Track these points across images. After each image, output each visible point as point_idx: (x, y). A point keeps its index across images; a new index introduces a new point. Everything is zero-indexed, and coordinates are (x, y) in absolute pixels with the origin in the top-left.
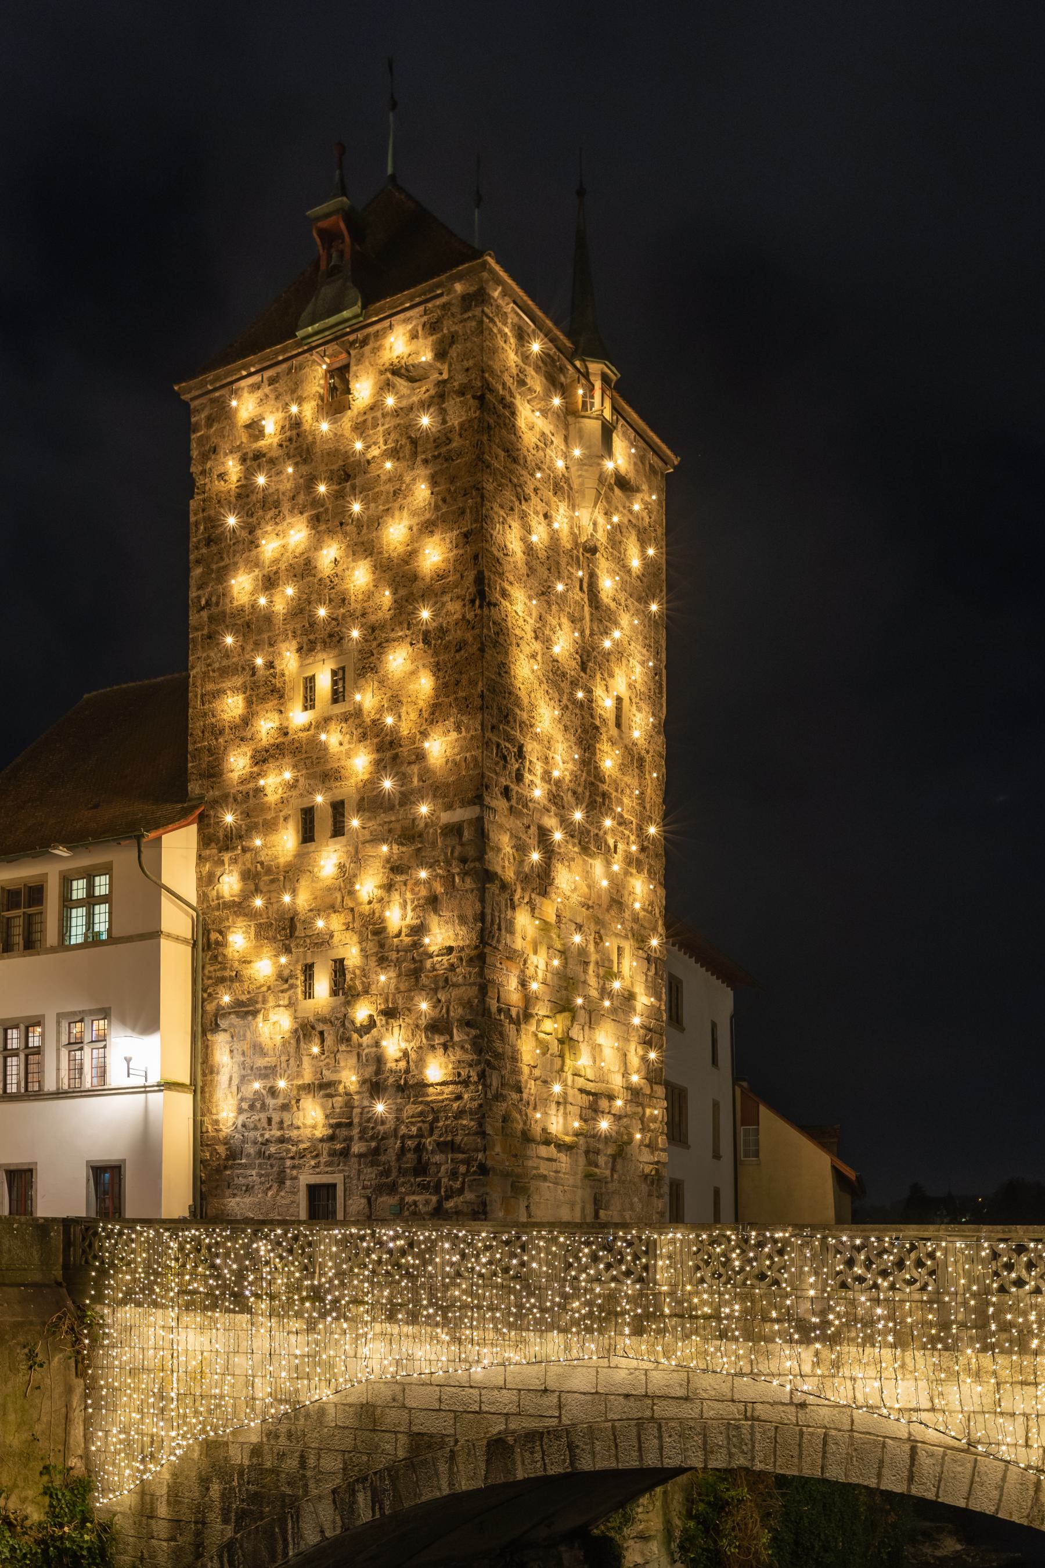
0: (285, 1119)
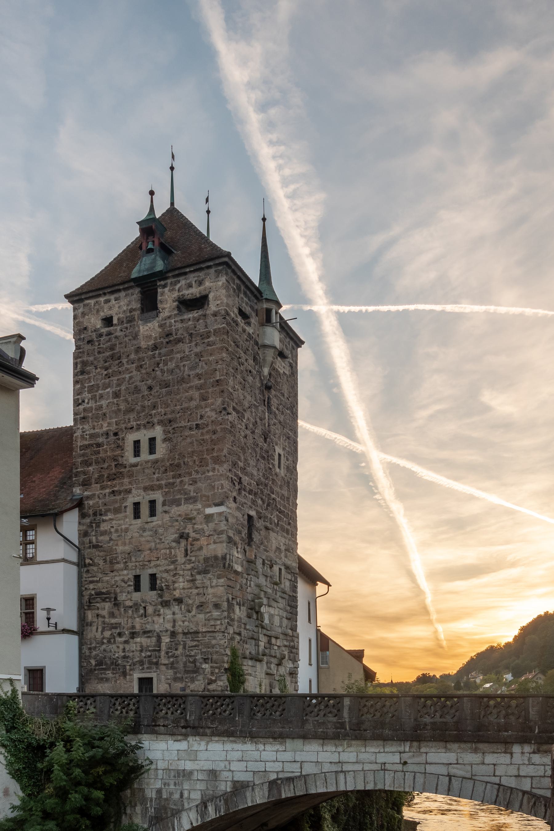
0: (126, 647)
